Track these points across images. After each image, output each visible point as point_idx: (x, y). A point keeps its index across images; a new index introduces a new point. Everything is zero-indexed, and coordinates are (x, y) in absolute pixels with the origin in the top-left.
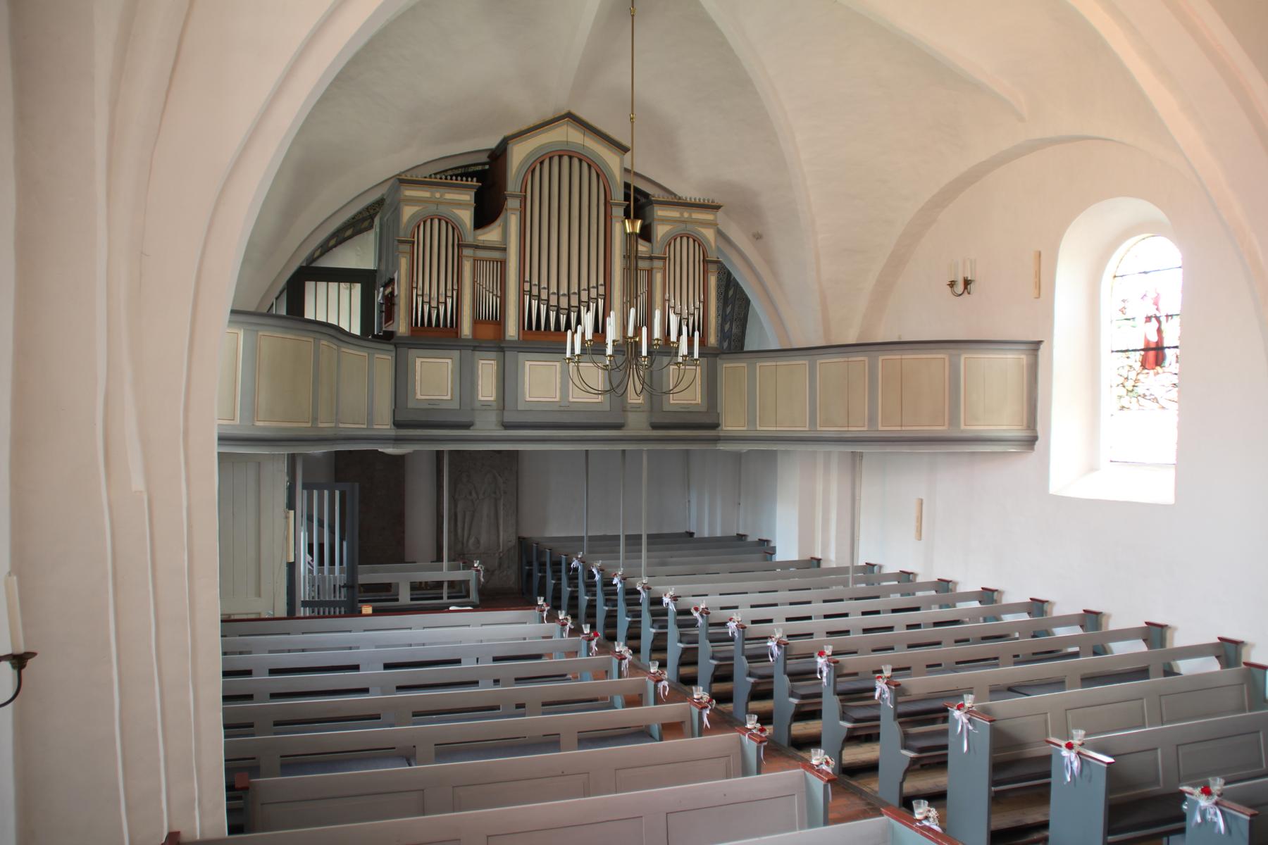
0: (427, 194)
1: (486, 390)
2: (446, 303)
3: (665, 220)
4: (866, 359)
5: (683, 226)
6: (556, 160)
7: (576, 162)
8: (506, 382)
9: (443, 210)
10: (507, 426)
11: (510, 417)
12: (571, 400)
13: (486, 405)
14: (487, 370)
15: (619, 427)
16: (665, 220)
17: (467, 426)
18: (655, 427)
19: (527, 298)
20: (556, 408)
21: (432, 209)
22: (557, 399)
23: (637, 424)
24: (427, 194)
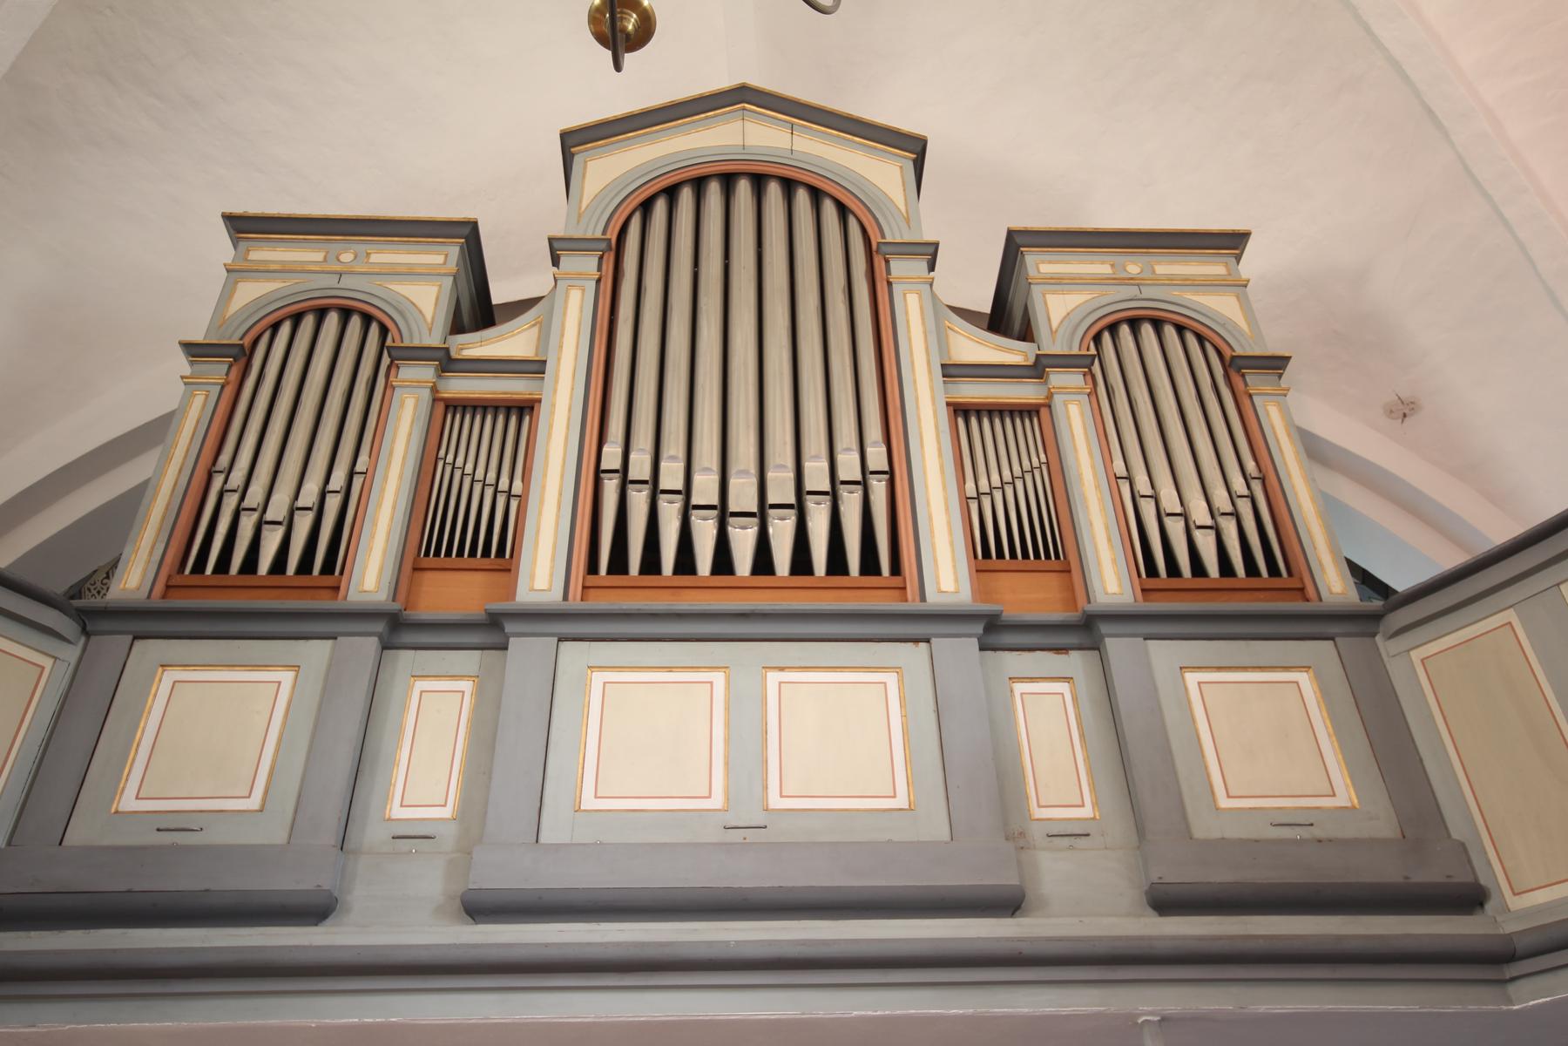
0: (1104, 269)
1: (424, 773)
2: (1236, 515)
3: (1059, 282)
4: (1510, 615)
5: (1133, 291)
6: (686, 195)
7: (802, 197)
8: (508, 757)
9: (356, 287)
10: (478, 909)
11: (504, 873)
12: (775, 802)
13: (415, 837)
14: (1046, 709)
15: (1009, 904)
16: (1060, 283)
17: (316, 911)
18: (1165, 903)
19: (611, 487)
20: (713, 835)
21: (1118, 298)
22: (717, 802)
23: (1086, 897)
24: (1104, 269)
